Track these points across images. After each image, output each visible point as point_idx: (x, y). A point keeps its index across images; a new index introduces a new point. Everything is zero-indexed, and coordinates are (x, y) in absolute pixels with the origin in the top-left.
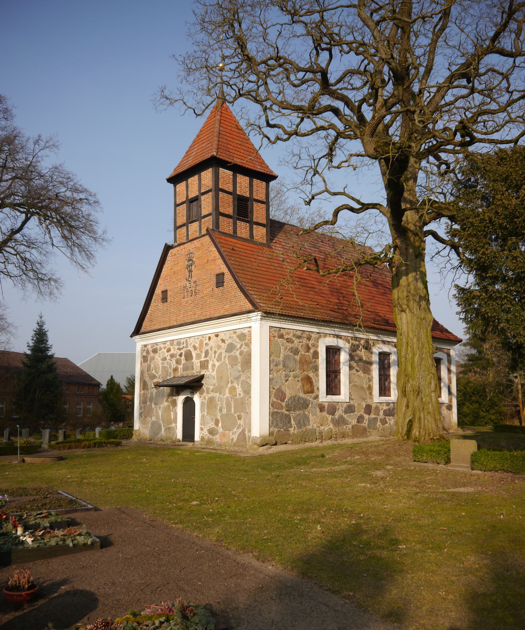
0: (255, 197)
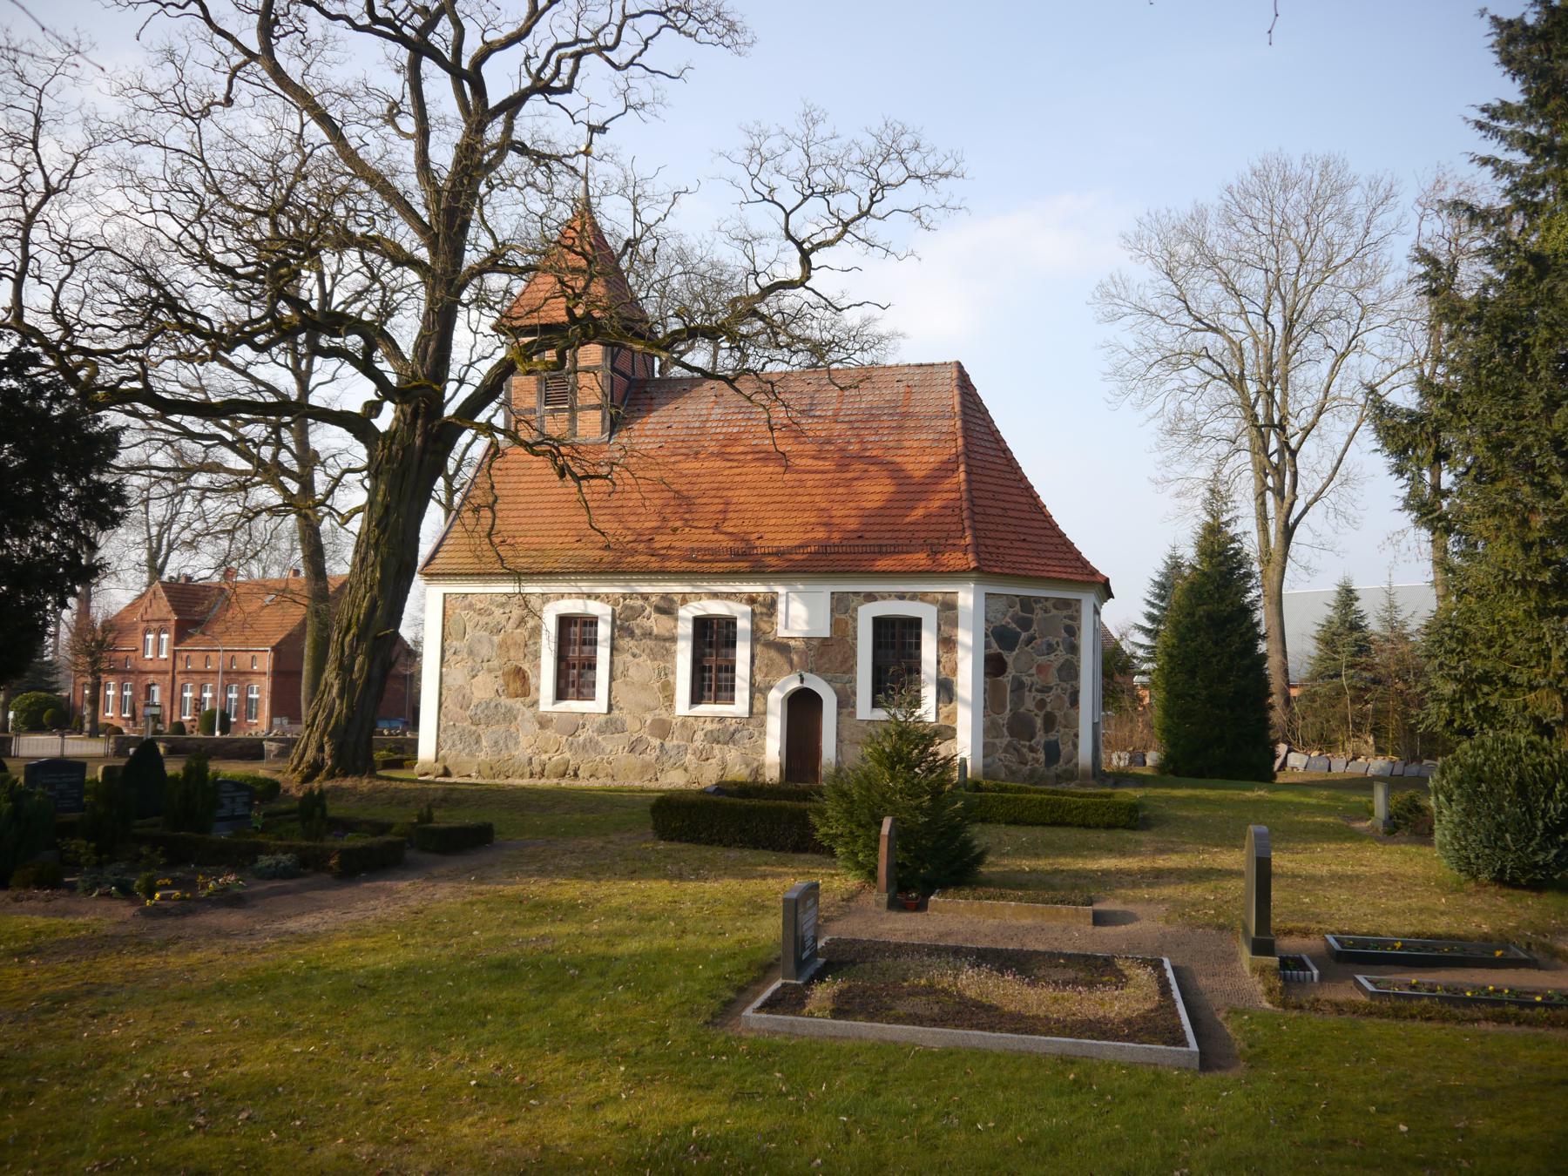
0: (314, 400)
